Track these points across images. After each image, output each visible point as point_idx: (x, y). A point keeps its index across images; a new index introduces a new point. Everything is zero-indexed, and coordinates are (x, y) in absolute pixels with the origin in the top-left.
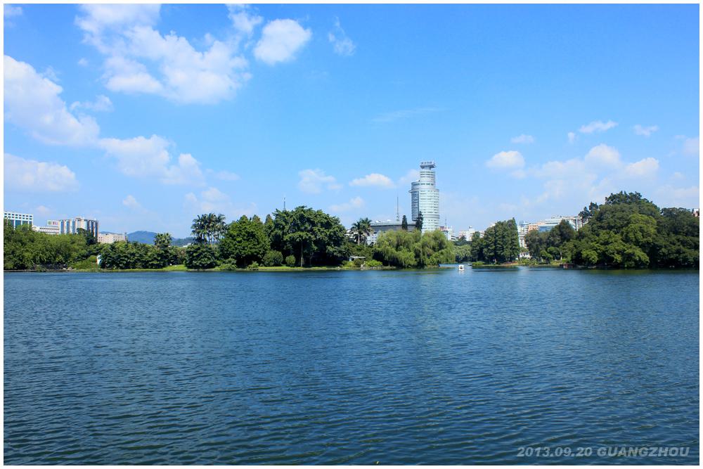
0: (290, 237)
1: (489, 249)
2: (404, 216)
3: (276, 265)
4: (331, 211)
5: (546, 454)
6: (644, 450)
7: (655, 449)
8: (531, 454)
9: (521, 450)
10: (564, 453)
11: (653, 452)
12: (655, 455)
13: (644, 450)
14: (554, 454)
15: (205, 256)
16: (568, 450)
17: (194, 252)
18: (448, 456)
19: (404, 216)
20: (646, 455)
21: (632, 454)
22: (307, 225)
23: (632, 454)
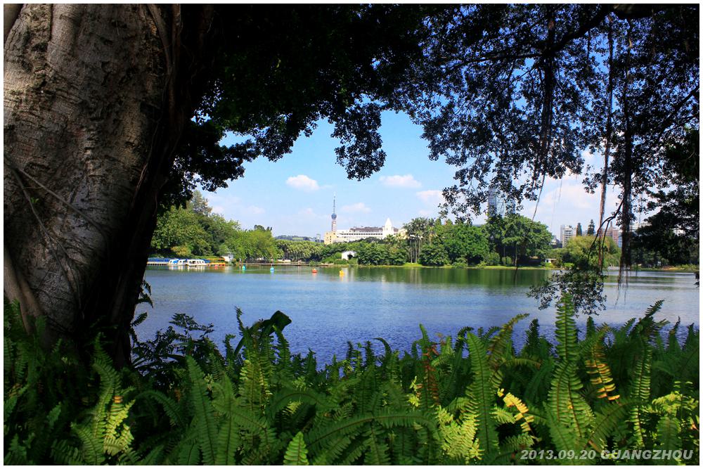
0: (509, 241)
1: (649, 255)
2: (579, 224)
3: (494, 265)
4: (252, 278)
5: (549, 456)
6: (647, 453)
7: (659, 452)
8: (535, 457)
9: (525, 453)
10: (567, 456)
11: (656, 455)
12: (659, 458)
13: (647, 453)
14: (558, 457)
15: (440, 256)
16: (571, 453)
17: (432, 252)
18: (434, 462)
19: (579, 224)
20: (649, 458)
21: (638, 453)
22: (522, 230)
23: (638, 453)
